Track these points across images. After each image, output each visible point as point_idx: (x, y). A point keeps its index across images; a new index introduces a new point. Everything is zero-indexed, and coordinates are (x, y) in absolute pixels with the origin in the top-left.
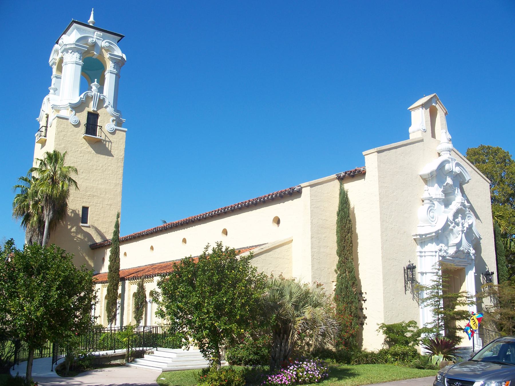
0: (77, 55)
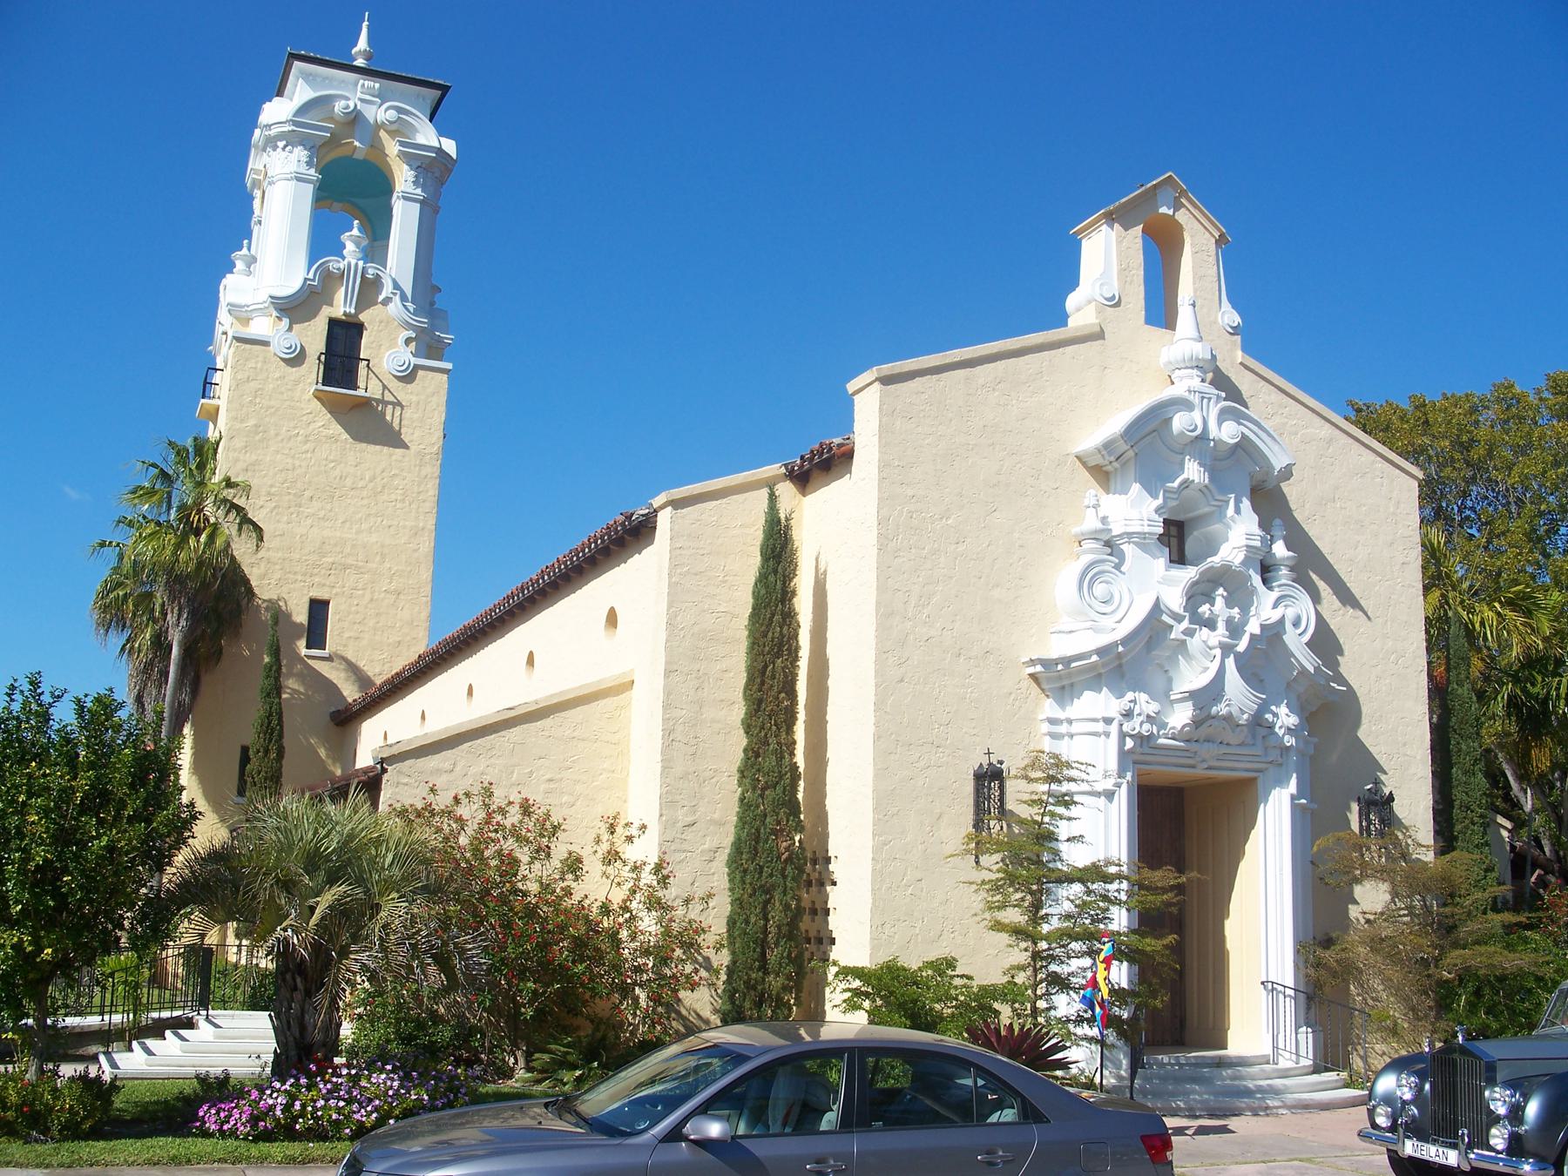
0: (300, 153)
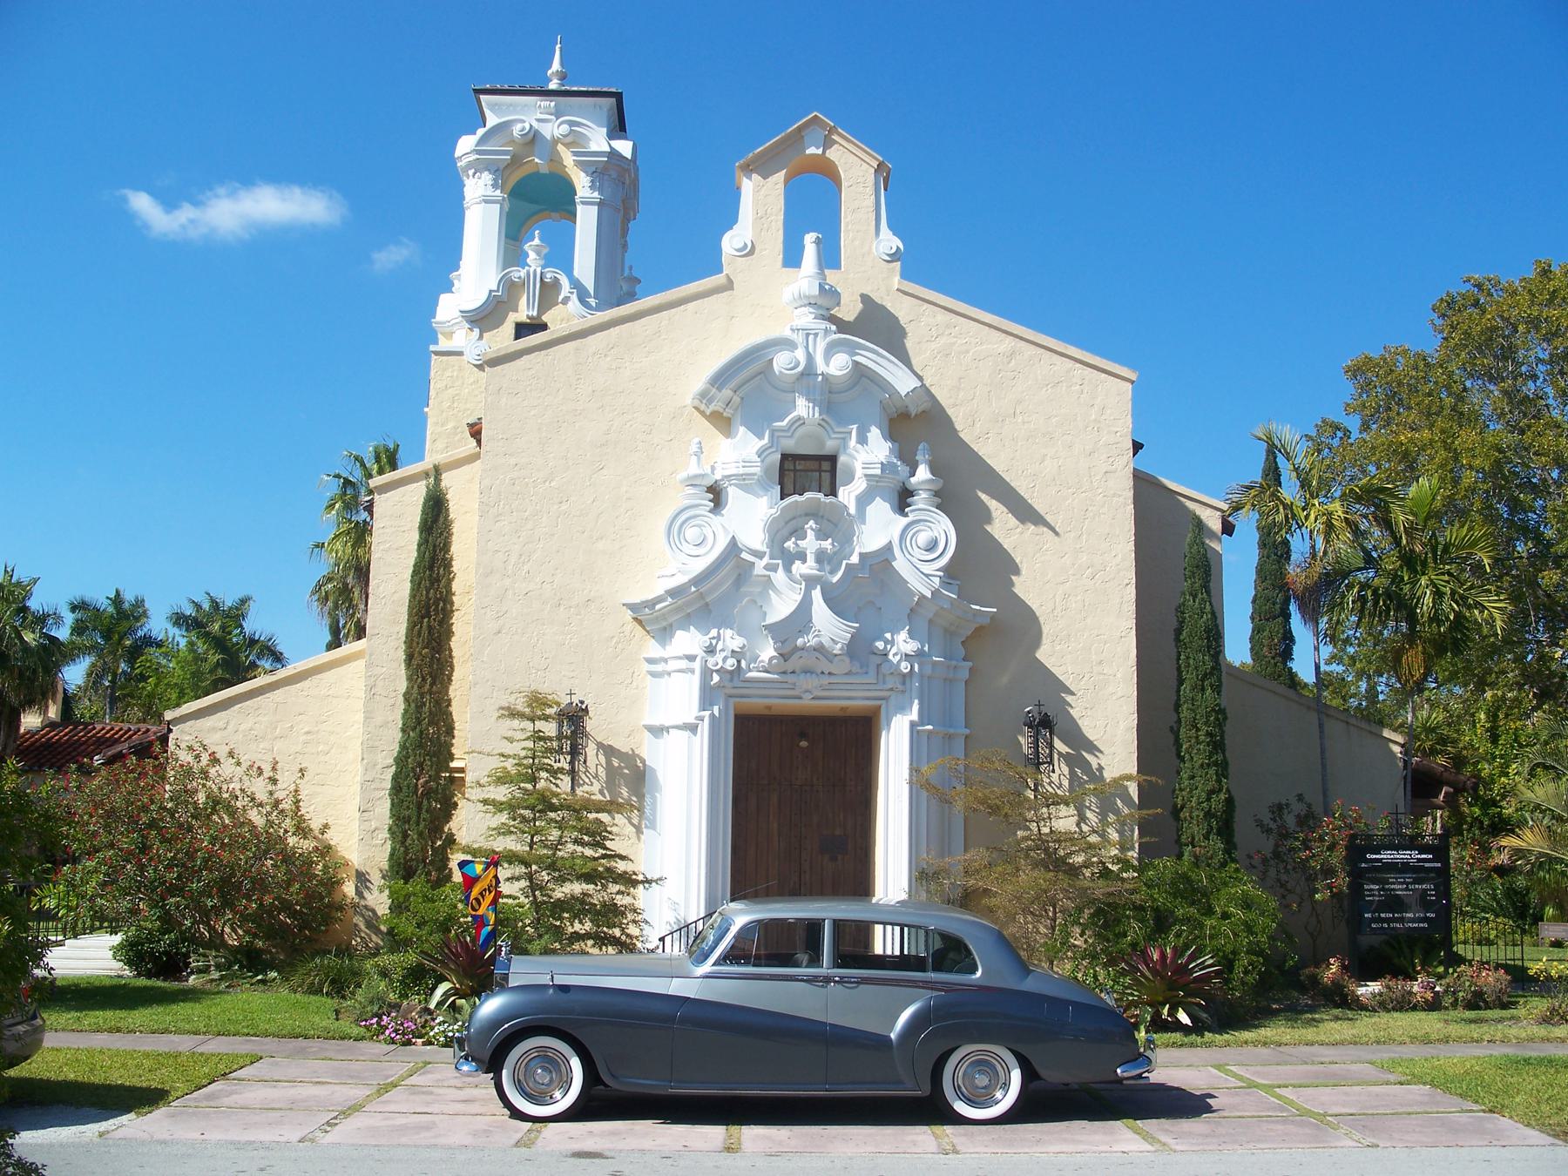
0: (487, 177)
